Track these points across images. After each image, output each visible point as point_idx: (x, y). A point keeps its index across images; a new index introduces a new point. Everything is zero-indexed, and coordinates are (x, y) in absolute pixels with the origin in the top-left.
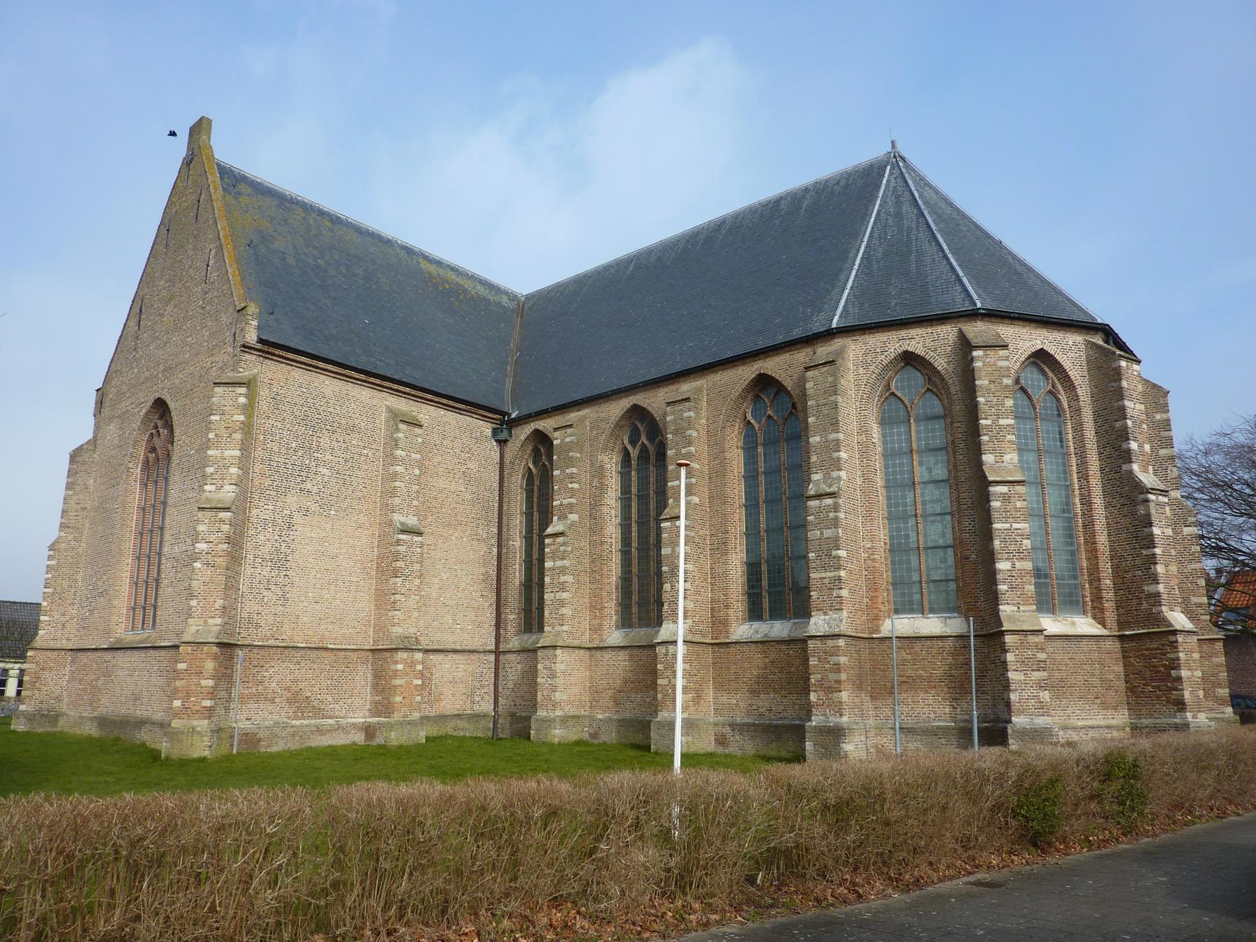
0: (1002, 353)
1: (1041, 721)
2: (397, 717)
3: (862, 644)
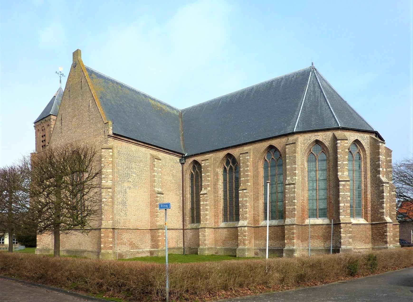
0: (346, 141)
1: (349, 247)
2: (160, 249)
3: (300, 227)
